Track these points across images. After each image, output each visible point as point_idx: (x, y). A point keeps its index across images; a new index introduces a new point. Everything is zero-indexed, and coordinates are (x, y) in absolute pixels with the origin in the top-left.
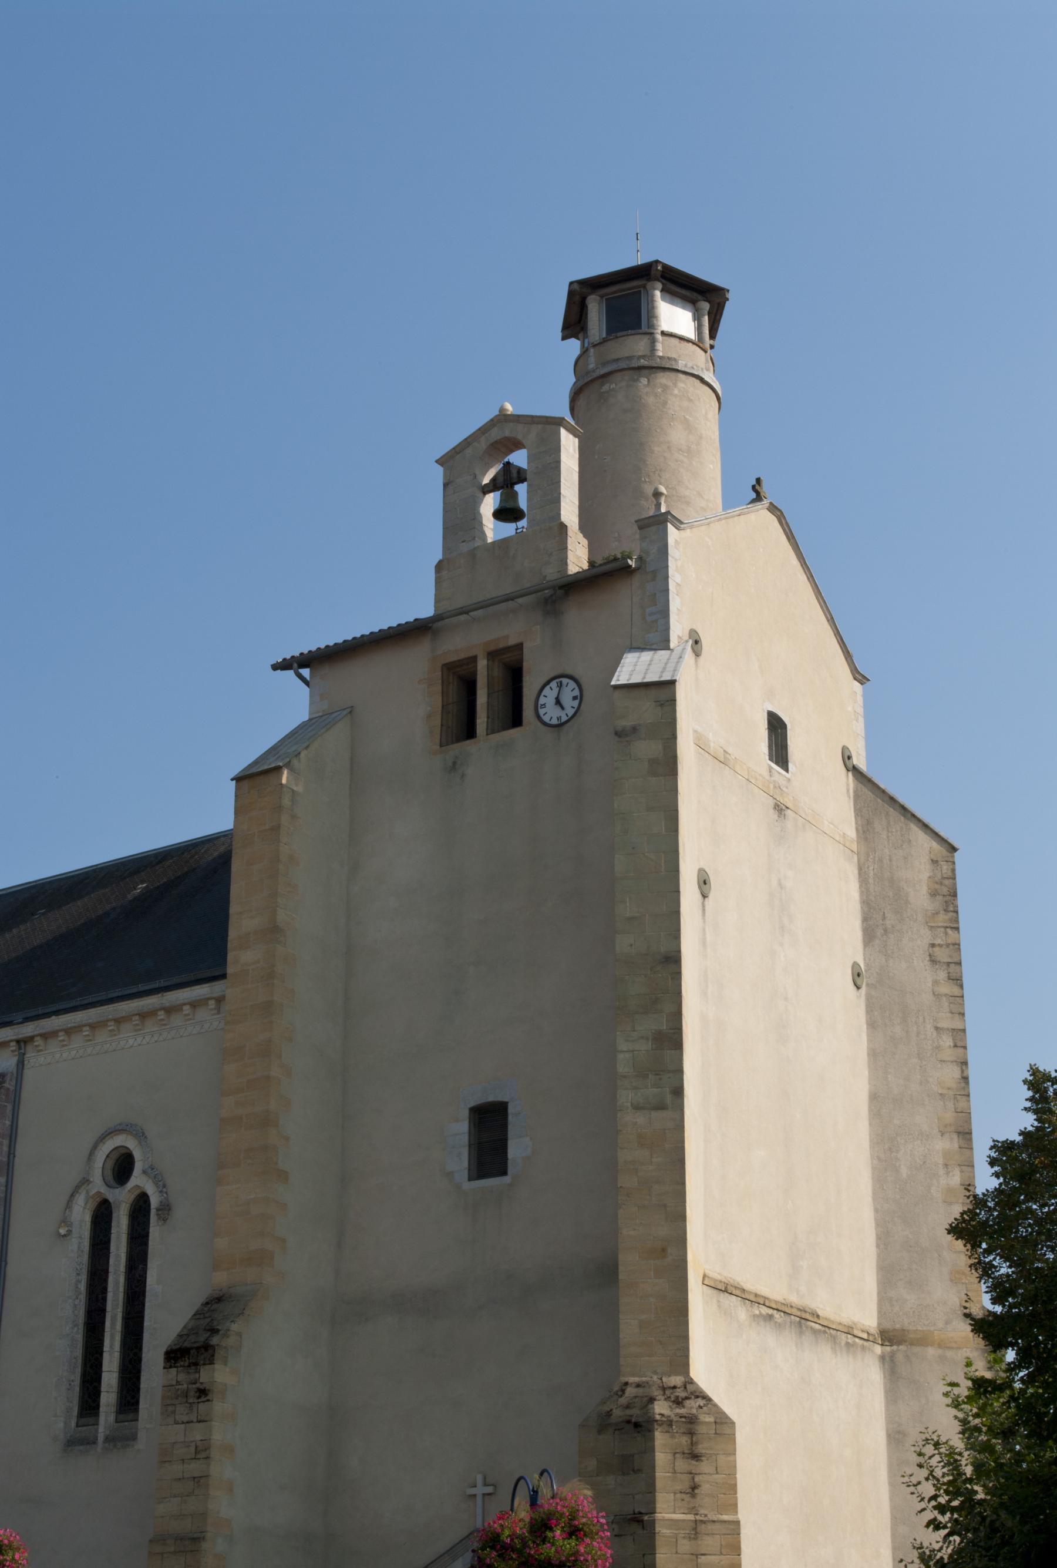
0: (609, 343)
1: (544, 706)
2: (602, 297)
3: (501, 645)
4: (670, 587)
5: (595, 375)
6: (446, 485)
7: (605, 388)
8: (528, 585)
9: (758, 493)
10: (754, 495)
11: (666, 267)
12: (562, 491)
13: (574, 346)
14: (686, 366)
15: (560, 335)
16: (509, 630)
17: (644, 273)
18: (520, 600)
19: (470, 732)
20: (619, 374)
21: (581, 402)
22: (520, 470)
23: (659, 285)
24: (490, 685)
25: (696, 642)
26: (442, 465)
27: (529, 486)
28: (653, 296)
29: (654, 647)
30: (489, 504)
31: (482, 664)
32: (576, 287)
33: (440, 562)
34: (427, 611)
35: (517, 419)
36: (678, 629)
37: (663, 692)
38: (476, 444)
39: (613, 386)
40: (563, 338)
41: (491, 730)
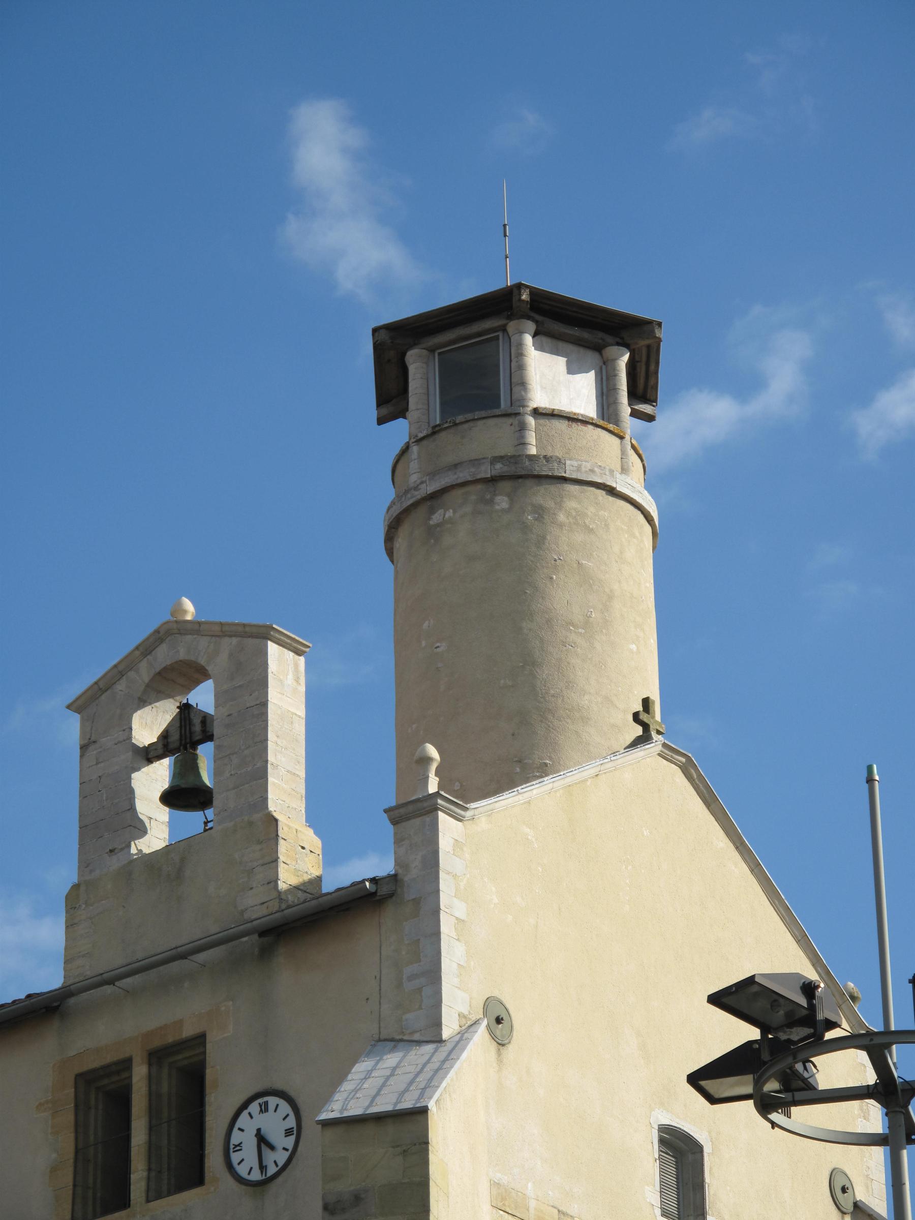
0: (443, 435)
1: (238, 1147)
2: (432, 350)
3: (170, 1039)
4: (444, 928)
5: (418, 495)
6: (84, 748)
7: (436, 518)
8: (214, 929)
9: (646, 727)
10: (639, 731)
11: (536, 294)
12: (271, 758)
13: (399, 431)
14: (579, 469)
15: (372, 412)
16: (182, 1012)
17: (500, 306)
18: (202, 957)
19: (122, 1201)
20: (459, 492)
21: (400, 543)
22: (206, 719)
23: (531, 326)
24: (153, 1112)
25: (499, 1020)
26: (78, 710)
27: (217, 748)
28: (520, 345)
29: (416, 1037)
30: (152, 781)
31: (140, 1073)
32: (384, 336)
33: (76, 887)
34: (50, 979)
35: (196, 628)
36: (457, 1001)
37: (407, 1127)
38: (132, 674)
39: (450, 513)
40: (381, 421)
41: (154, 1194)
